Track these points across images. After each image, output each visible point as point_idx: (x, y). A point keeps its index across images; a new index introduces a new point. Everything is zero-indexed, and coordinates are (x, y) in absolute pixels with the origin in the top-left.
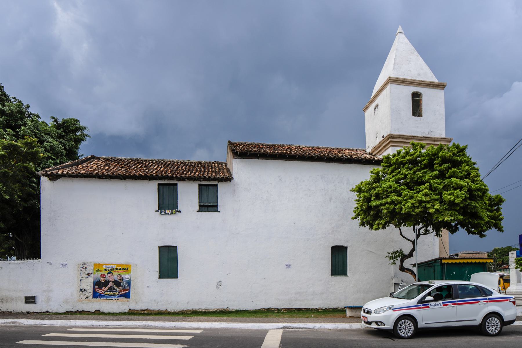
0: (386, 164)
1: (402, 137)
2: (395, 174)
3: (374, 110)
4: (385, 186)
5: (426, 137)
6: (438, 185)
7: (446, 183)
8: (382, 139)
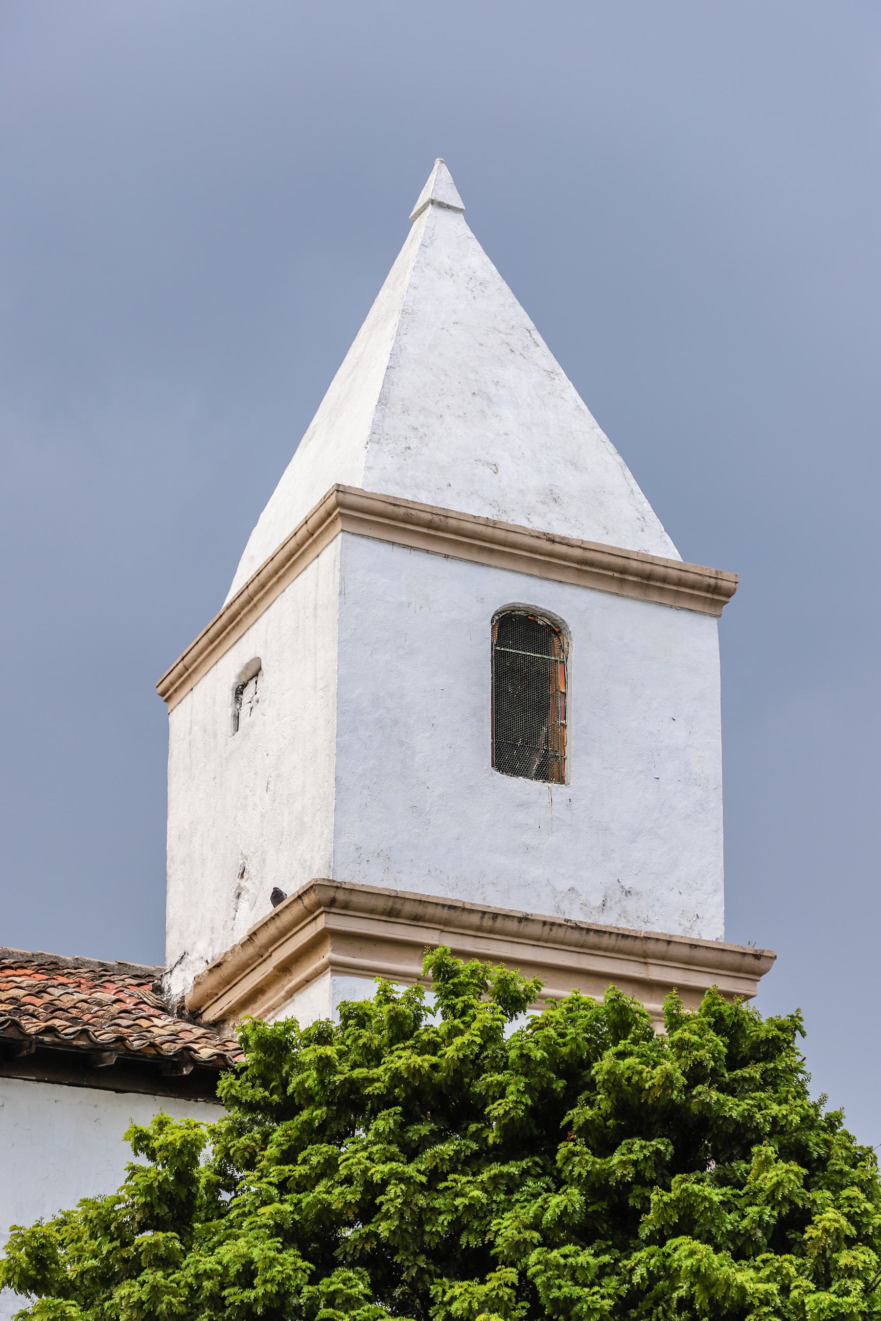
0: (260, 1093)
1: (408, 908)
2: (300, 1170)
3: (229, 695)
4: (208, 1263)
5: (588, 930)
6: (585, 1285)
7: (636, 1279)
8: (268, 909)
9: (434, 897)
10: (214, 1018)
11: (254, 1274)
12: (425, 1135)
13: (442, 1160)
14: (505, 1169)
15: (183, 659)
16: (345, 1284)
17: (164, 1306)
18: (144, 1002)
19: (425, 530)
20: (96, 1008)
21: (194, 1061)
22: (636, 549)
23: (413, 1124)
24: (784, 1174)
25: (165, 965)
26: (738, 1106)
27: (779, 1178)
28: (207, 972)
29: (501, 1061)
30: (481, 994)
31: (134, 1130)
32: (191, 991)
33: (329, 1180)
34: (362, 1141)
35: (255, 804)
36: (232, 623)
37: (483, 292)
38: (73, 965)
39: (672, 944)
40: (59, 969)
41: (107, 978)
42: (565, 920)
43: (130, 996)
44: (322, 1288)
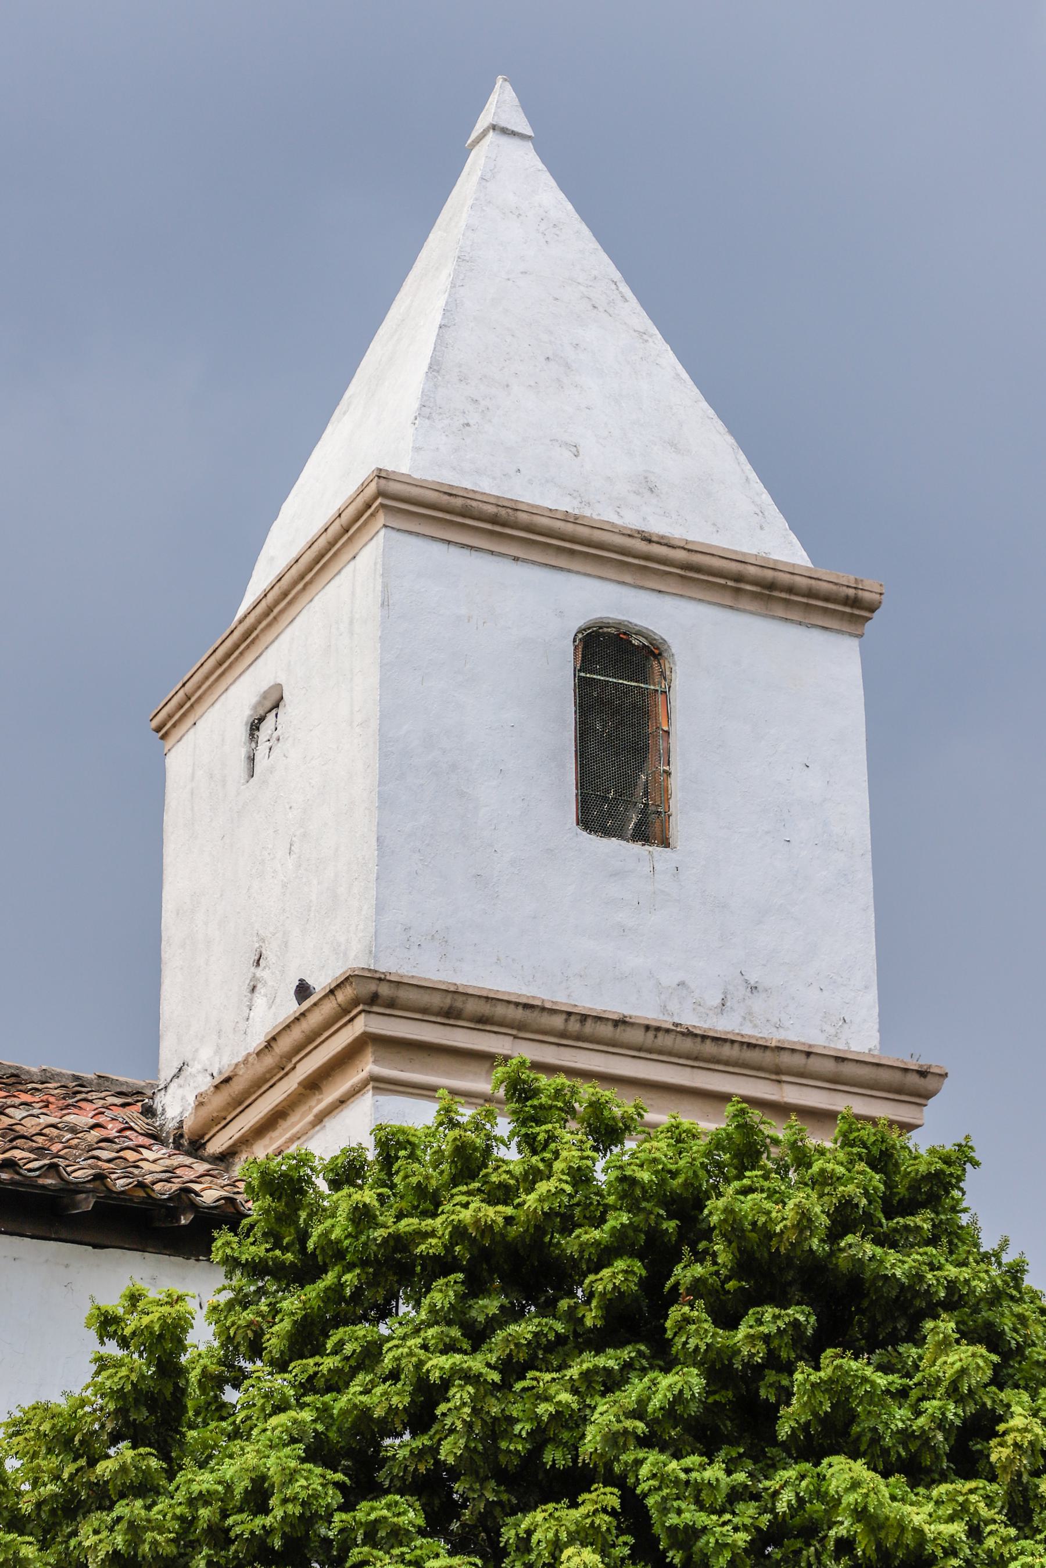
1: (472, 1007)
2: (329, 1363)
3: (243, 732)
5: (704, 1038)
6: (713, 1511)
7: (782, 1507)
8: (291, 1007)
9: (504, 993)
10: (220, 1150)
11: (267, 1495)
12: (494, 1314)
13: (518, 1345)
14: (601, 1361)
15: (184, 685)
16: (388, 1510)
17: (147, 1547)
18: (131, 1128)
19: (489, 526)
20: (69, 1136)
21: (194, 1207)
22: (754, 552)
23: (476, 1296)
24: (970, 1359)
25: (158, 1079)
26: (903, 1262)
27: (964, 1363)
28: (212, 1089)
29: (597, 1210)
30: (566, 1121)
31: (96, 1312)
32: (191, 1114)
33: (367, 1372)
34: (413, 1320)
35: (275, 871)
36: (245, 640)
37: (557, 235)
38: (40, 1078)
39: (812, 1056)
40: (21, 1083)
41: (83, 1096)
42: (674, 1024)
43: (113, 1119)
44: (360, 1515)
